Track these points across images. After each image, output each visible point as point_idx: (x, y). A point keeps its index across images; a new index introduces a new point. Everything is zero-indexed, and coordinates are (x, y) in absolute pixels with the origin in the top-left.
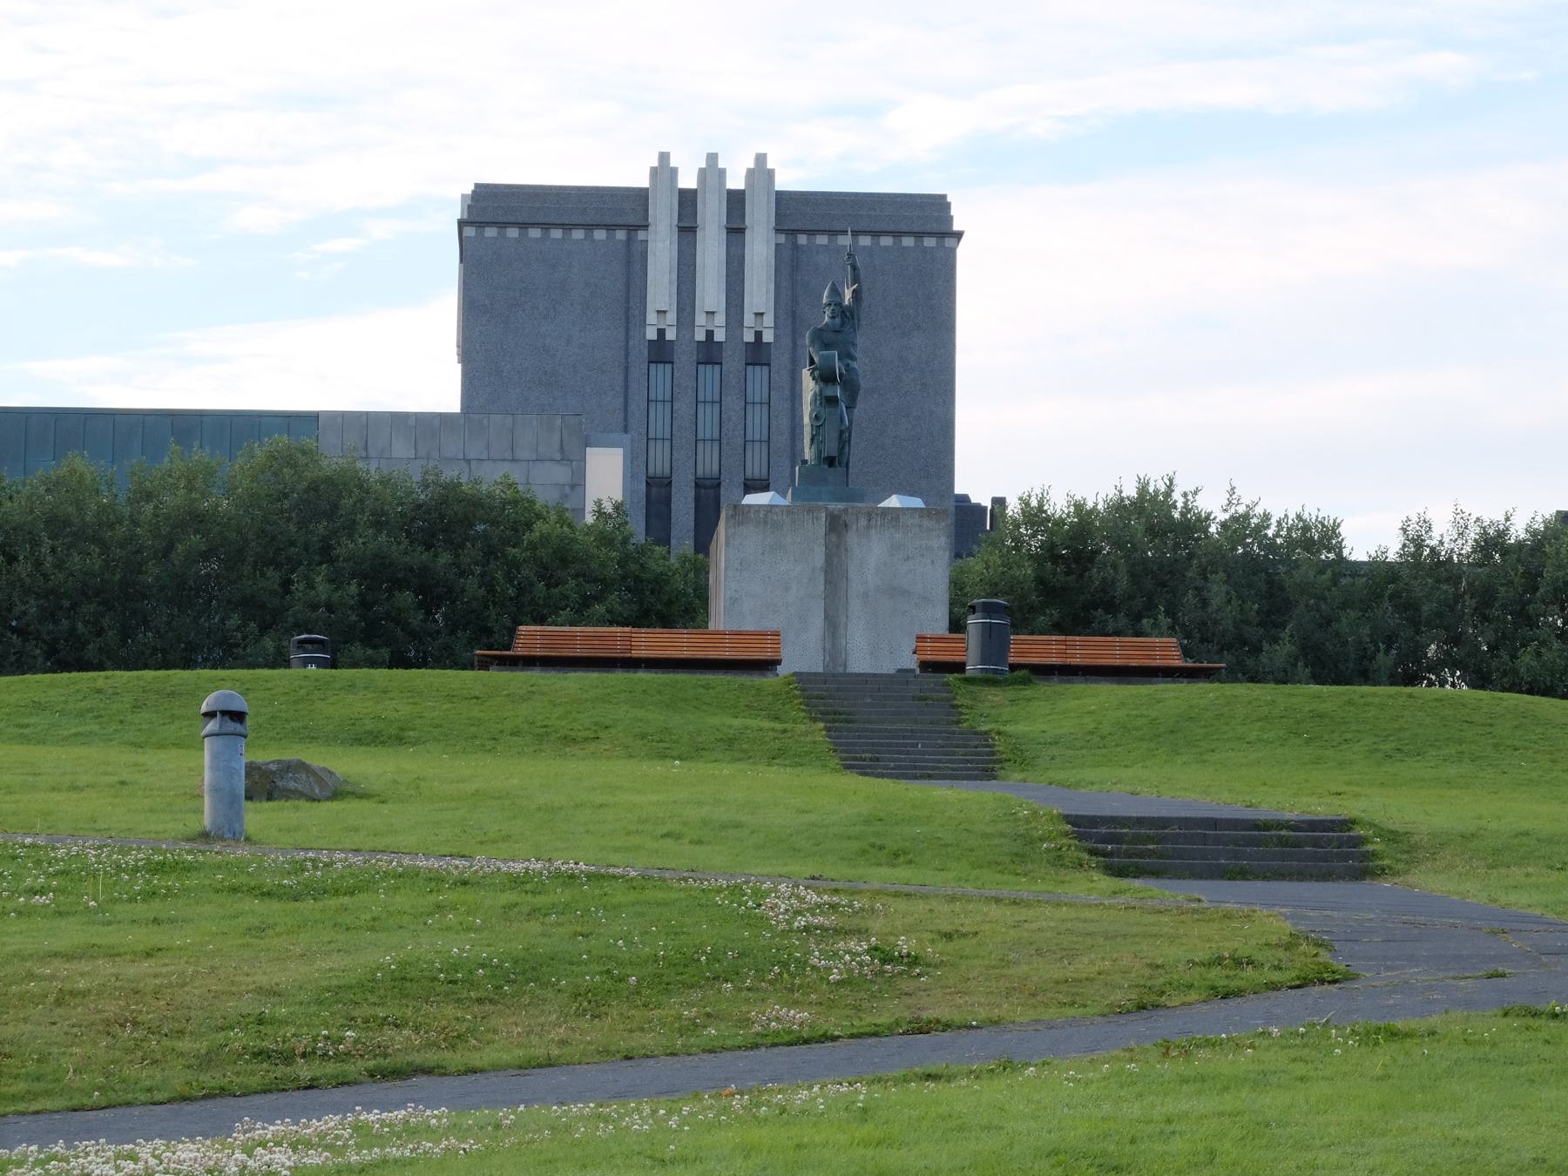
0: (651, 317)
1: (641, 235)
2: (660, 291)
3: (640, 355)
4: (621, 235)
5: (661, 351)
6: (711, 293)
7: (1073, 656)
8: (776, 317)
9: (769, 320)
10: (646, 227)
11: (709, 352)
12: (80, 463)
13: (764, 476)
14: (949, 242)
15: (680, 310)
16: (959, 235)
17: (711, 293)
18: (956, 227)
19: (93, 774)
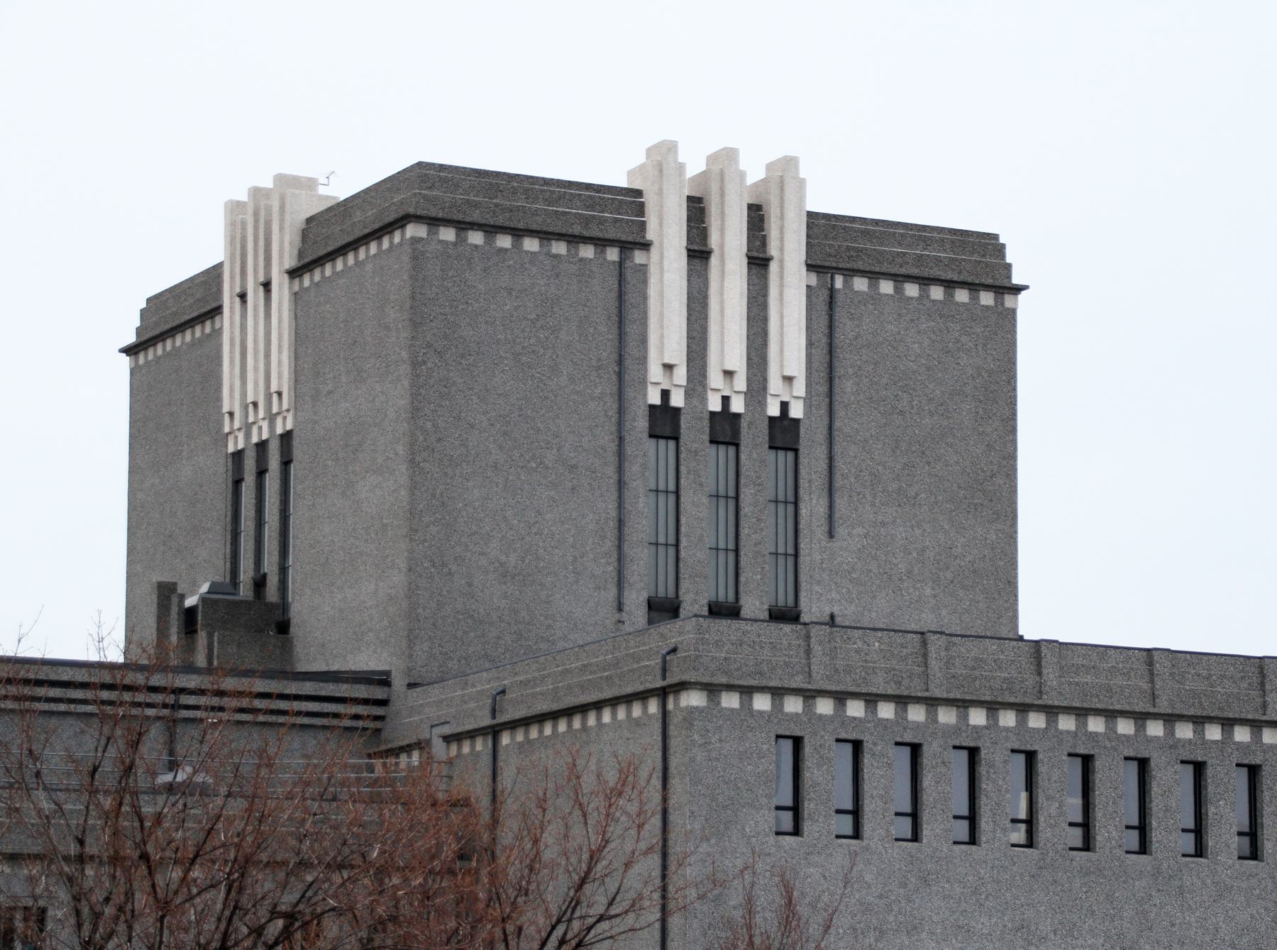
0: (655, 372)
1: (639, 257)
2: (666, 338)
3: (641, 423)
4: (613, 254)
5: (665, 421)
6: (729, 347)
7: (930, 776)
8: (809, 385)
9: (800, 388)
10: (646, 246)
11: (725, 428)
12: (358, 216)
13: (671, 594)
14: (1008, 301)
15: (690, 360)
16: (1018, 289)
17: (729, 347)
18: (1016, 280)
19: (674, 946)
